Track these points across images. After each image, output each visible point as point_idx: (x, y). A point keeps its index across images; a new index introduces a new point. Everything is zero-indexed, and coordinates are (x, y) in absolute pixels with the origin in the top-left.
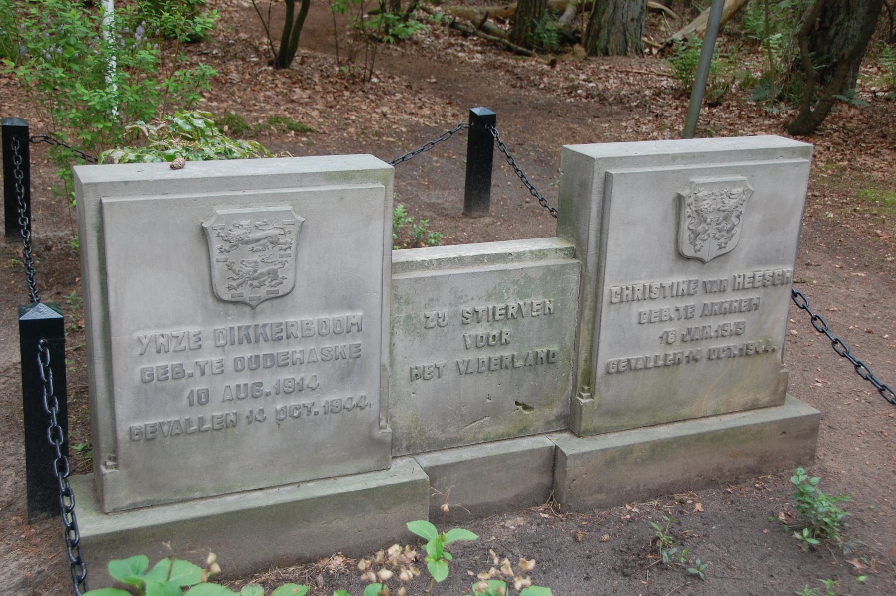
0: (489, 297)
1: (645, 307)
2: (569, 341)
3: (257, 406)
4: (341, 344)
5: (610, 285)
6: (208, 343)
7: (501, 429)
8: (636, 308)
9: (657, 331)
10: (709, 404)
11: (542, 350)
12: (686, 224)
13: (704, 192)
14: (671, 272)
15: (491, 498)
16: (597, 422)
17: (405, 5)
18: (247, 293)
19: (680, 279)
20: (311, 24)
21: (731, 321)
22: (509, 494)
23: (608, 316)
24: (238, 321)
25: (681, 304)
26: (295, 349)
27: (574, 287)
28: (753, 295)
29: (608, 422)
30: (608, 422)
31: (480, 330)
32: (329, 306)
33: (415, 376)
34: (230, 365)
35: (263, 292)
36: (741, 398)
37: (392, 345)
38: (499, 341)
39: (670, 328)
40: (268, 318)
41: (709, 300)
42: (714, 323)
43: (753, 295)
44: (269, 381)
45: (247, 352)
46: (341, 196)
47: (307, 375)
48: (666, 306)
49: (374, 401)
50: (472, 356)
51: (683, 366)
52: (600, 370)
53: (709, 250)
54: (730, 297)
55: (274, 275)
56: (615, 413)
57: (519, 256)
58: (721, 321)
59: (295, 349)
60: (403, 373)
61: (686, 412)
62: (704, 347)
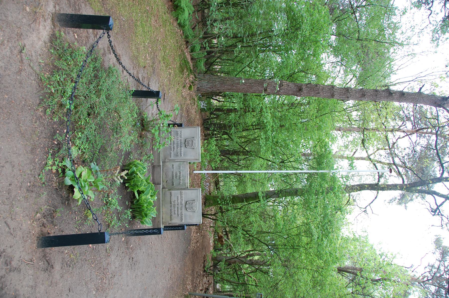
0: (183, 175)
1: (180, 197)
2: (175, 187)
3: (173, 144)
4: (179, 153)
5: (183, 191)
6: (181, 138)
7: (164, 178)
8: (180, 196)
9: (176, 200)
10: (164, 210)
11: (174, 183)
12: (191, 202)
13: (196, 203)
14: (184, 201)
15: (155, 175)
16: (164, 191)
17: (1, 27)
18: (186, 142)
19: (183, 203)
20: (82, 111)
21: (176, 212)
22: (155, 178)
23: (179, 191)
24: (183, 141)
25: (180, 203)
26: (179, 148)
27: (183, 187)
28: (180, 215)
29: (163, 193)
30: (163, 193)
31: (178, 174)
32: (184, 152)
33: (173, 165)
34: (178, 141)
35: (186, 144)
36: (164, 216)
37: (177, 162)
38: (176, 176)
39: (176, 201)
40: (183, 145)
41: (180, 208)
42: (176, 209)
43: (180, 215)
44: (175, 145)
45: (179, 143)
46: (197, 154)
47: (175, 150)
48: (179, 201)
49: (171, 158)
50: (175, 173)
51: (170, 205)
52: (171, 191)
53: (187, 206)
54: (180, 211)
55: (188, 145)
56: (164, 194)
57: (187, 180)
58: (176, 210)
59: (179, 148)
60: (174, 163)
61: (163, 206)
62: (173, 208)
